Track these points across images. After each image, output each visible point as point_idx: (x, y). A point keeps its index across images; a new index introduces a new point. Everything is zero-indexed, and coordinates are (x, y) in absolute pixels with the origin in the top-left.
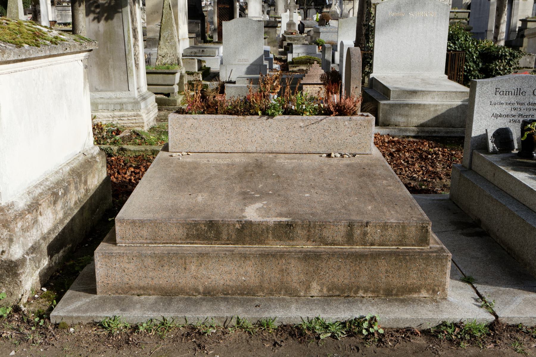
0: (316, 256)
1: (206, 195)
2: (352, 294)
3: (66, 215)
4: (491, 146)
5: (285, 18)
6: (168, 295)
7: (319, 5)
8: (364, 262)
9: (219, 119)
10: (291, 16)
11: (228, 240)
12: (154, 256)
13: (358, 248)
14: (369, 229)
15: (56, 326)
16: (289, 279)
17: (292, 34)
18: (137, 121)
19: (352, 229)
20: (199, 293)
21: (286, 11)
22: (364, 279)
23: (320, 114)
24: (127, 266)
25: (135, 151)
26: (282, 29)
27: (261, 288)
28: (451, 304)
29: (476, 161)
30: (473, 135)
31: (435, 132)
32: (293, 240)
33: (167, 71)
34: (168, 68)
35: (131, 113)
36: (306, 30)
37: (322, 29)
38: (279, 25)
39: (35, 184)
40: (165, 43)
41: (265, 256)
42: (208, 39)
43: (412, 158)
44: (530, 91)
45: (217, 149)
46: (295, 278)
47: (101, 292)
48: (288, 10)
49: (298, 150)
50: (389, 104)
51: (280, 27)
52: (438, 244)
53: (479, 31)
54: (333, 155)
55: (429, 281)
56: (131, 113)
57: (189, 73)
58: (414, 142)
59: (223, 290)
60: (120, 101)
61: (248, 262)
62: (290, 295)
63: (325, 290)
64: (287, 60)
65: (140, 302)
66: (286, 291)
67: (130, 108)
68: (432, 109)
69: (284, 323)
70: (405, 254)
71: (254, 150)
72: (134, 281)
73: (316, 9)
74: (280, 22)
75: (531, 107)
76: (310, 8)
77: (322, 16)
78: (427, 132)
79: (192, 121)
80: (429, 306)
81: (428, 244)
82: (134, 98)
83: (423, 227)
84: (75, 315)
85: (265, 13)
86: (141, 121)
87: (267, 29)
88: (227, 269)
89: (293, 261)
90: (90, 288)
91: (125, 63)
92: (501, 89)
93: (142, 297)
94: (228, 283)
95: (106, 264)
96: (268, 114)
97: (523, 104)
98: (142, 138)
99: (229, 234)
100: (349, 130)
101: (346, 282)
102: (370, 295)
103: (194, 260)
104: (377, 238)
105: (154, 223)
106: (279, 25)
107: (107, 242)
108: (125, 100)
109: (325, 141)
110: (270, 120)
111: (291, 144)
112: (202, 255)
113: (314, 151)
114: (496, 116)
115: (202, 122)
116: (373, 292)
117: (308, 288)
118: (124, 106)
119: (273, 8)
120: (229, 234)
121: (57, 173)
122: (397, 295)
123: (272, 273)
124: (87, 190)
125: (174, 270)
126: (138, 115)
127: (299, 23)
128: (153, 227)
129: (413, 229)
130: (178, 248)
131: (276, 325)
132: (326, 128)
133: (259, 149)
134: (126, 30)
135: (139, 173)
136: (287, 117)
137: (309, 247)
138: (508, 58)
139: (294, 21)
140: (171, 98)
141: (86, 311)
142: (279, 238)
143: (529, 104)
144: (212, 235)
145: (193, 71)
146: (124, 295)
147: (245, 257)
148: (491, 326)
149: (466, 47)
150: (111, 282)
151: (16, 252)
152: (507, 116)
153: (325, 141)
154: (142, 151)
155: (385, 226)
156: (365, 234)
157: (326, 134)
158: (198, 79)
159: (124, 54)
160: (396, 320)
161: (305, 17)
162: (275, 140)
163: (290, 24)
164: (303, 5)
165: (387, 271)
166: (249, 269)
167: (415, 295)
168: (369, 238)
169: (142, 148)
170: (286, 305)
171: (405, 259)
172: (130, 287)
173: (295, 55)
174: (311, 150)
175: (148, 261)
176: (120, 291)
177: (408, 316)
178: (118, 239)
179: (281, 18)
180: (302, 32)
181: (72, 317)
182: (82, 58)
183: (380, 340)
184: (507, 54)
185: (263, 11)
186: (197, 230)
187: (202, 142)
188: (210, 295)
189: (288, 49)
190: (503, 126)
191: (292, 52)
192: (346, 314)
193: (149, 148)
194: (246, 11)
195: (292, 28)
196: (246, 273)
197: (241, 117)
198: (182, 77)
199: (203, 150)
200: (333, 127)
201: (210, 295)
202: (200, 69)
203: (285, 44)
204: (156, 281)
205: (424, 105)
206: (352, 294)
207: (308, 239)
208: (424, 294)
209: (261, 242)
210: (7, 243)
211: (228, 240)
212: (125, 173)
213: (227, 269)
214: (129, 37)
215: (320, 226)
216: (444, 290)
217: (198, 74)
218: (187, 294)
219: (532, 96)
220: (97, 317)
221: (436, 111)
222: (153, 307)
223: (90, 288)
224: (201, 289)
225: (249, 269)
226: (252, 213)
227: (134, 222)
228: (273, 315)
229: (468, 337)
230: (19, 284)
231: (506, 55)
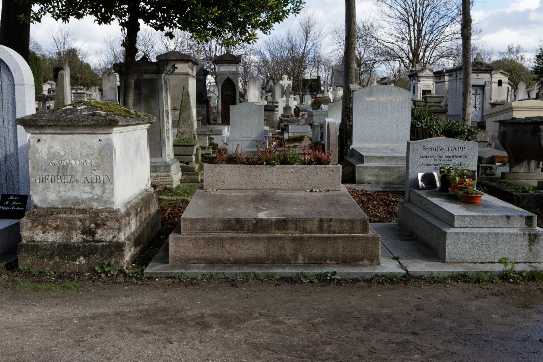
0: (301, 239)
1: (233, 209)
2: (323, 262)
4: (421, 184)
5: (281, 103)
6: (211, 262)
7: (314, 91)
8: (329, 242)
9: (238, 168)
10: (287, 101)
11: (248, 230)
12: (204, 239)
13: (326, 235)
14: (332, 223)
15: (148, 278)
16: (285, 253)
17: (288, 116)
18: (168, 180)
19: (322, 223)
20: (231, 262)
21: (282, 97)
22: (330, 253)
23: (305, 163)
24: (188, 245)
25: (168, 200)
26: (280, 112)
27: (268, 258)
28: (382, 267)
29: (412, 195)
30: (410, 178)
31: (399, 188)
32: (287, 230)
33: (187, 144)
34: (188, 142)
35: (163, 174)
36: (301, 113)
37: (315, 112)
38: (276, 109)
39: (126, 202)
40: (183, 122)
41: (269, 238)
42: (212, 122)
43: (379, 204)
44: (446, 148)
45: (236, 187)
46: (289, 252)
47: (172, 262)
48: (284, 96)
49: (290, 188)
50: (363, 167)
51: (278, 111)
52: (374, 232)
53: (456, 114)
54: (314, 190)
55: (368, 254)
56: (163, 174)
57: (203, 148)
58: (382, 195)
59: (245, 260)
60: (155, 164)
61: (260, 242)
62: (286, 263)
63: (306, 260)
64: (284, 138)
65: (195, 266)
66: (283, 261)
67: (162, 170)
68: (396, 170)
69: (282, 276)
70: (353, 237)
71: (261, 188)
72: (192, 255)
73: (311, 94)
74: (277, 107)
75: (447, 159)
76: (305, 94)
77: (315, 100)
78: (393, 188)
79: (219, 168)
80: (369, 268)
81: (368, 232)
82: (166, 163)
83: (364, 222)
84: (158, 271)
85: (263, 98)
86: (171, 180)
87: (267, 113)
88: (247, 247)
89: (287, 242)
90: (165, 259)
91: (159, 136)
93: (197, 265)
94: (248, 255)
95: (175, 244)
96: (270, 164)
97: (442, 157)
98: (173, 192)
99: (248, 227)
100: (325, 174)
101: (319, 254)
102: (333, 263)
103: (228, 241)
104: (337, 228)
105: (204, 220)
106: (276, 109)
107: (174, 233)
108: (159, 164)
109: (309, 181)
110: (272, 168)
111: (286, 184)
112: (232, 238)
113: (301, 188)
115: (226, 170)
116: (335, 261)
117: (296, 258)
118: (158, 169)
119: (270, 94)
120: (248, 227)
121: (135, 198)
122: (350, 262)
123: (274, 250)
124: (149, 214)
125: (216, 248)
126: (168, 176)
127: (295, 107)
128: (203, 224)
129: (359, 223)
131: (277, 277)
132: (309, 173)
133: (264, 187)
134: (161, 111)
135: (174, 213)
136: (283, 165)
137: (297, 234)
138: (466, 134)
140: (190, 166)
141: (165, 270)
142: (278, 229)
143: (446, 157)
144: (238, 227)
145: (205, 146)
146: (186, 262)
147: (258, 239)
148: (404, 276)
149: (431, 125)
150: (178, 255)
151: (122, 237)
153: (309, 181)
154: (174, 200)
155: (342, 221)
156: (330, 226)
158: (209, 152)
159: (159, 129)
160: (348, 274)
161: (302, 101)
162: (275, 181)
163: (287, 108)
164: (299, 91)
165: (343, 248)
166: (261, 247)
167: (361, 263)
168: (332, 229)
169: (174, 198)
170: (284, 267)
171: (354, 240)
172: (189, 259)
173: (291, 135)
174: (299, 188)
175: (201, 242)
176: (183, 261)
177: (355, 271)
178: (182, 230)
179: (277, 103)
180: (297, 115)
181: (156, 273)
182: (147, 128)
183: (338, 283)
184: (466, 130)
185: (261, 98)
186: (229, 224)
187: (226, 182)
188: (237, 262)
189: (285, 129)
190: (429, 172)
191: (288, 132)
192: (318, 270)
193: (179, 198)
194: (246, 97)
195: (288, 111)
196: (258, 249)
197: (252, 166)
198: (197, 150)
199: (227, 188)
200: (314, 172)
201: (237, 262)
202: (211, 144)
203: (282, 125)
204: (205, 255)
205: (390, 167)
206: (323, 262)
207: (296, 230)
208: (366, 262)
209: (268, 232)
210: (117, 231)
211: (248, 230)
212: (165, 214)
213: (247, 247)
214: (163, 116)
215: (303, 221)
216: (378, 259)
217: (209, 148)
218: (223, 263)
220: (171, 273)
221: (399, 172)
222: (204, 268)
223: (165, 259)
224: (232, 259)
225: (261, 247)
226: (262, 215)
227: (192, 220)
228: (275, 271)
229: (389, 281)
230: (122, 256)
231: (465, 132)
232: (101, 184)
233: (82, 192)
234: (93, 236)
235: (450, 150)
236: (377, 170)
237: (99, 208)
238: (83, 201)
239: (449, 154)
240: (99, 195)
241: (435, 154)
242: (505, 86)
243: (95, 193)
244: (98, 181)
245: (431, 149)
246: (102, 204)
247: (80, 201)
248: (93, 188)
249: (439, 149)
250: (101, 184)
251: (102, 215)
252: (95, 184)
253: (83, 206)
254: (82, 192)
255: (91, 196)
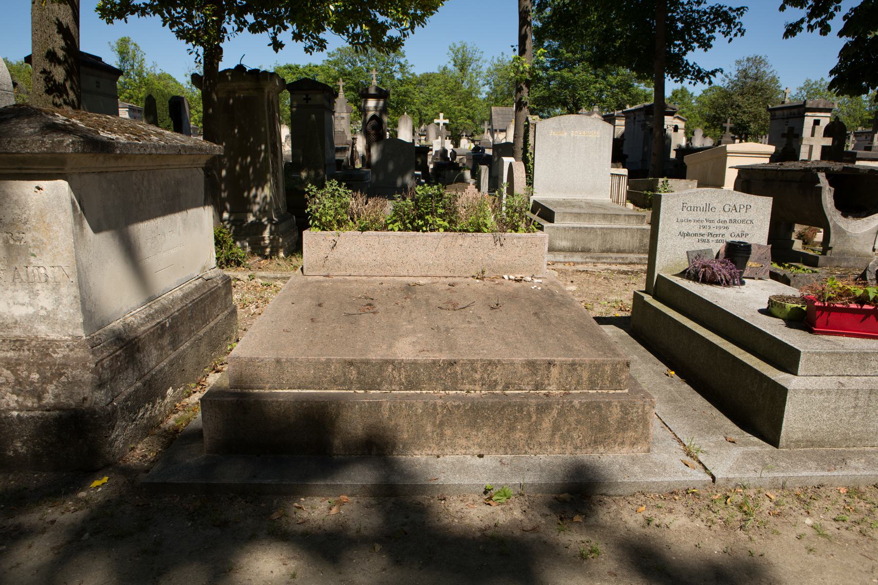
3: (712, 429)
21: (437, 138)
44: (719, 207)
75: (721, 224)
92: (688, 205)
97: (713, 221)
100: (518, 249)
114: (684, 235)
130: (30, 167)
139: (446, 148)
143: (719, 221)
152: (695, 235)
156: (856, 398)
157: (491, 254)
219: (722, 212)
232: (50, 286)
233: (11, 302)
234: (40, 398)
235: (727, 210)
236: (572, 232)
237: (53, 336)
238: (16, 322)
239: (725, 217)
240: (49, 309)
241: (702, 216)
242: (681, 132)
243: (40, 304)
244: (43, 279)
245: (695, 209)
246: (58, 328)
247: (10, 321)
248: (34, 294)
249: (708, 208)
250: (50, 286)
251: (55, 352)
252: (38, 287)
253: (17, 332)
254: (11, 302)
255: (31, 310)
